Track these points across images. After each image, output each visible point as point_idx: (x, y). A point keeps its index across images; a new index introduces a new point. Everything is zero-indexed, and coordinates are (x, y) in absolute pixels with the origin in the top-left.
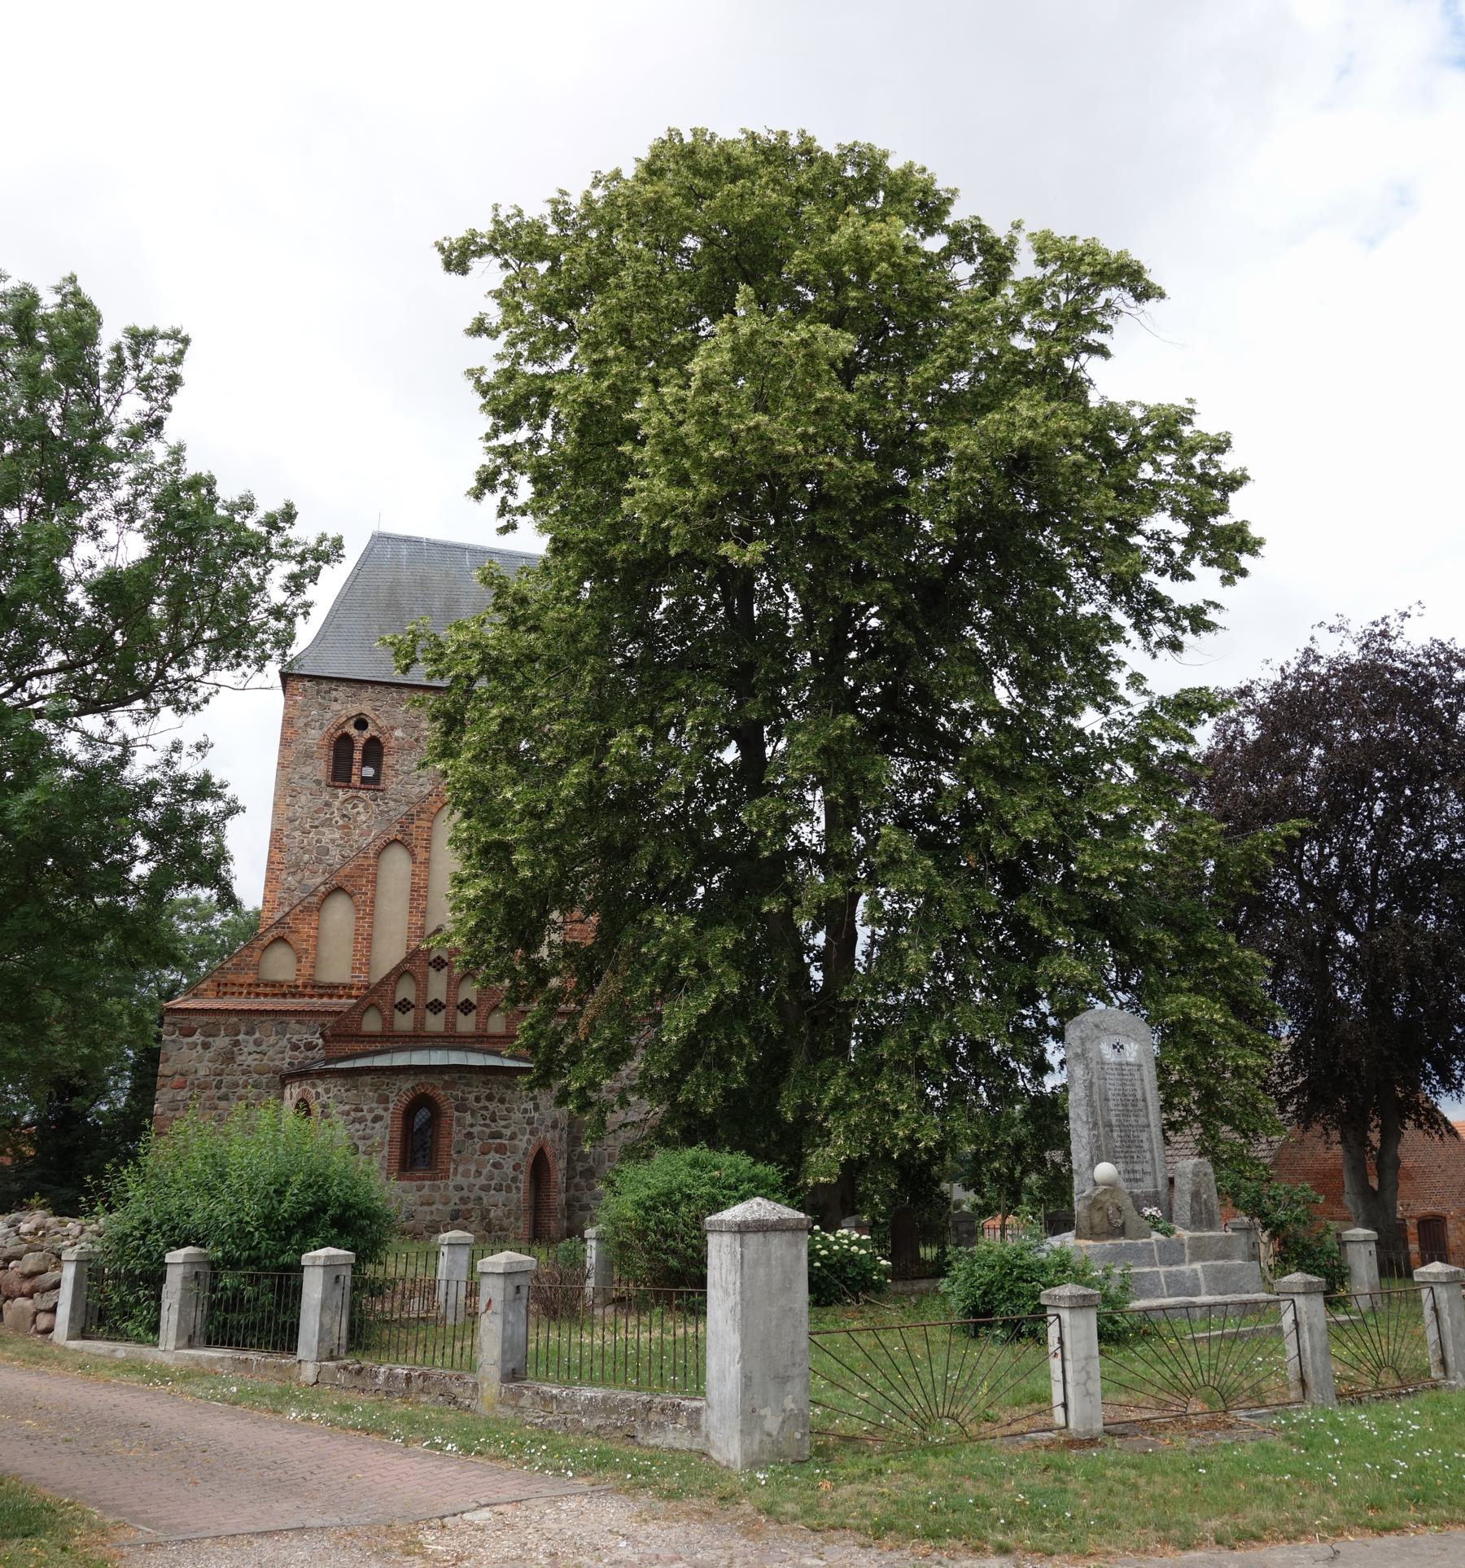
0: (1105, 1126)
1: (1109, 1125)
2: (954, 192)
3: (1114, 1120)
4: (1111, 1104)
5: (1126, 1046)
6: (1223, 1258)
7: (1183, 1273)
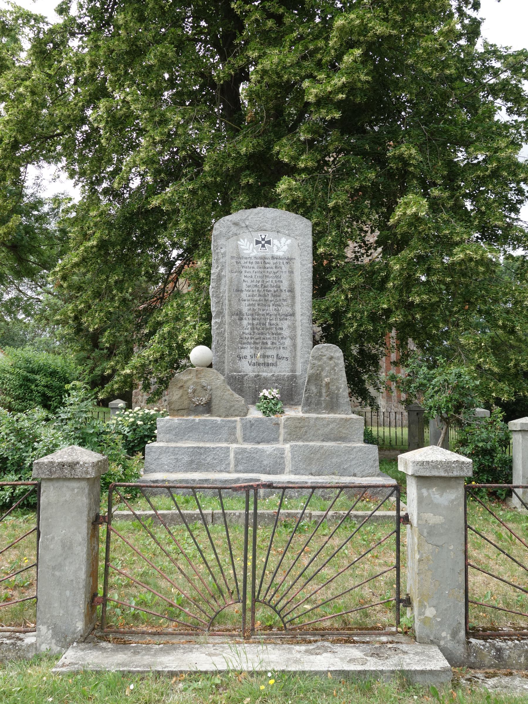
0: (232, 314)
1: (240, 315)
2: (483, 19)
3: (245, 309)
4: (244, 295)
5: (275, 242)
6: (335, 439)
7: (263, 451)
